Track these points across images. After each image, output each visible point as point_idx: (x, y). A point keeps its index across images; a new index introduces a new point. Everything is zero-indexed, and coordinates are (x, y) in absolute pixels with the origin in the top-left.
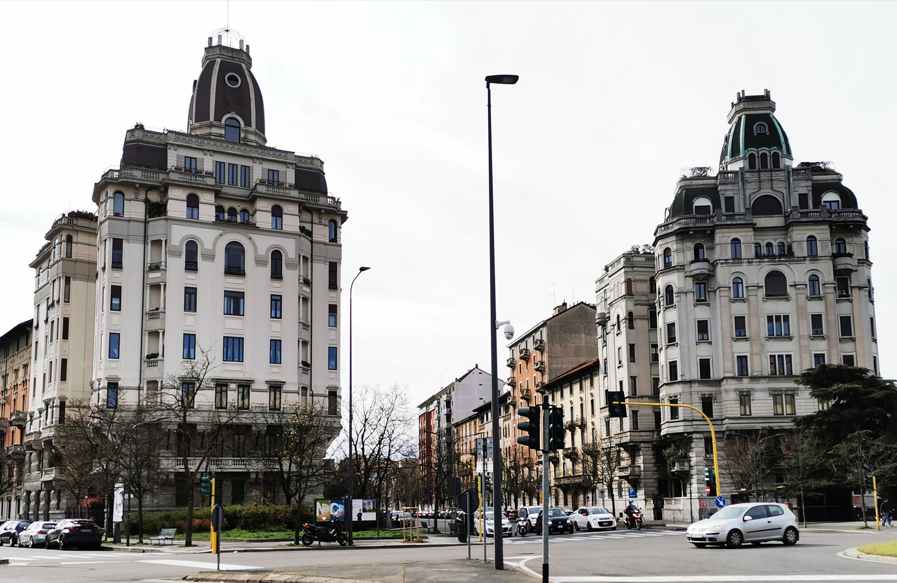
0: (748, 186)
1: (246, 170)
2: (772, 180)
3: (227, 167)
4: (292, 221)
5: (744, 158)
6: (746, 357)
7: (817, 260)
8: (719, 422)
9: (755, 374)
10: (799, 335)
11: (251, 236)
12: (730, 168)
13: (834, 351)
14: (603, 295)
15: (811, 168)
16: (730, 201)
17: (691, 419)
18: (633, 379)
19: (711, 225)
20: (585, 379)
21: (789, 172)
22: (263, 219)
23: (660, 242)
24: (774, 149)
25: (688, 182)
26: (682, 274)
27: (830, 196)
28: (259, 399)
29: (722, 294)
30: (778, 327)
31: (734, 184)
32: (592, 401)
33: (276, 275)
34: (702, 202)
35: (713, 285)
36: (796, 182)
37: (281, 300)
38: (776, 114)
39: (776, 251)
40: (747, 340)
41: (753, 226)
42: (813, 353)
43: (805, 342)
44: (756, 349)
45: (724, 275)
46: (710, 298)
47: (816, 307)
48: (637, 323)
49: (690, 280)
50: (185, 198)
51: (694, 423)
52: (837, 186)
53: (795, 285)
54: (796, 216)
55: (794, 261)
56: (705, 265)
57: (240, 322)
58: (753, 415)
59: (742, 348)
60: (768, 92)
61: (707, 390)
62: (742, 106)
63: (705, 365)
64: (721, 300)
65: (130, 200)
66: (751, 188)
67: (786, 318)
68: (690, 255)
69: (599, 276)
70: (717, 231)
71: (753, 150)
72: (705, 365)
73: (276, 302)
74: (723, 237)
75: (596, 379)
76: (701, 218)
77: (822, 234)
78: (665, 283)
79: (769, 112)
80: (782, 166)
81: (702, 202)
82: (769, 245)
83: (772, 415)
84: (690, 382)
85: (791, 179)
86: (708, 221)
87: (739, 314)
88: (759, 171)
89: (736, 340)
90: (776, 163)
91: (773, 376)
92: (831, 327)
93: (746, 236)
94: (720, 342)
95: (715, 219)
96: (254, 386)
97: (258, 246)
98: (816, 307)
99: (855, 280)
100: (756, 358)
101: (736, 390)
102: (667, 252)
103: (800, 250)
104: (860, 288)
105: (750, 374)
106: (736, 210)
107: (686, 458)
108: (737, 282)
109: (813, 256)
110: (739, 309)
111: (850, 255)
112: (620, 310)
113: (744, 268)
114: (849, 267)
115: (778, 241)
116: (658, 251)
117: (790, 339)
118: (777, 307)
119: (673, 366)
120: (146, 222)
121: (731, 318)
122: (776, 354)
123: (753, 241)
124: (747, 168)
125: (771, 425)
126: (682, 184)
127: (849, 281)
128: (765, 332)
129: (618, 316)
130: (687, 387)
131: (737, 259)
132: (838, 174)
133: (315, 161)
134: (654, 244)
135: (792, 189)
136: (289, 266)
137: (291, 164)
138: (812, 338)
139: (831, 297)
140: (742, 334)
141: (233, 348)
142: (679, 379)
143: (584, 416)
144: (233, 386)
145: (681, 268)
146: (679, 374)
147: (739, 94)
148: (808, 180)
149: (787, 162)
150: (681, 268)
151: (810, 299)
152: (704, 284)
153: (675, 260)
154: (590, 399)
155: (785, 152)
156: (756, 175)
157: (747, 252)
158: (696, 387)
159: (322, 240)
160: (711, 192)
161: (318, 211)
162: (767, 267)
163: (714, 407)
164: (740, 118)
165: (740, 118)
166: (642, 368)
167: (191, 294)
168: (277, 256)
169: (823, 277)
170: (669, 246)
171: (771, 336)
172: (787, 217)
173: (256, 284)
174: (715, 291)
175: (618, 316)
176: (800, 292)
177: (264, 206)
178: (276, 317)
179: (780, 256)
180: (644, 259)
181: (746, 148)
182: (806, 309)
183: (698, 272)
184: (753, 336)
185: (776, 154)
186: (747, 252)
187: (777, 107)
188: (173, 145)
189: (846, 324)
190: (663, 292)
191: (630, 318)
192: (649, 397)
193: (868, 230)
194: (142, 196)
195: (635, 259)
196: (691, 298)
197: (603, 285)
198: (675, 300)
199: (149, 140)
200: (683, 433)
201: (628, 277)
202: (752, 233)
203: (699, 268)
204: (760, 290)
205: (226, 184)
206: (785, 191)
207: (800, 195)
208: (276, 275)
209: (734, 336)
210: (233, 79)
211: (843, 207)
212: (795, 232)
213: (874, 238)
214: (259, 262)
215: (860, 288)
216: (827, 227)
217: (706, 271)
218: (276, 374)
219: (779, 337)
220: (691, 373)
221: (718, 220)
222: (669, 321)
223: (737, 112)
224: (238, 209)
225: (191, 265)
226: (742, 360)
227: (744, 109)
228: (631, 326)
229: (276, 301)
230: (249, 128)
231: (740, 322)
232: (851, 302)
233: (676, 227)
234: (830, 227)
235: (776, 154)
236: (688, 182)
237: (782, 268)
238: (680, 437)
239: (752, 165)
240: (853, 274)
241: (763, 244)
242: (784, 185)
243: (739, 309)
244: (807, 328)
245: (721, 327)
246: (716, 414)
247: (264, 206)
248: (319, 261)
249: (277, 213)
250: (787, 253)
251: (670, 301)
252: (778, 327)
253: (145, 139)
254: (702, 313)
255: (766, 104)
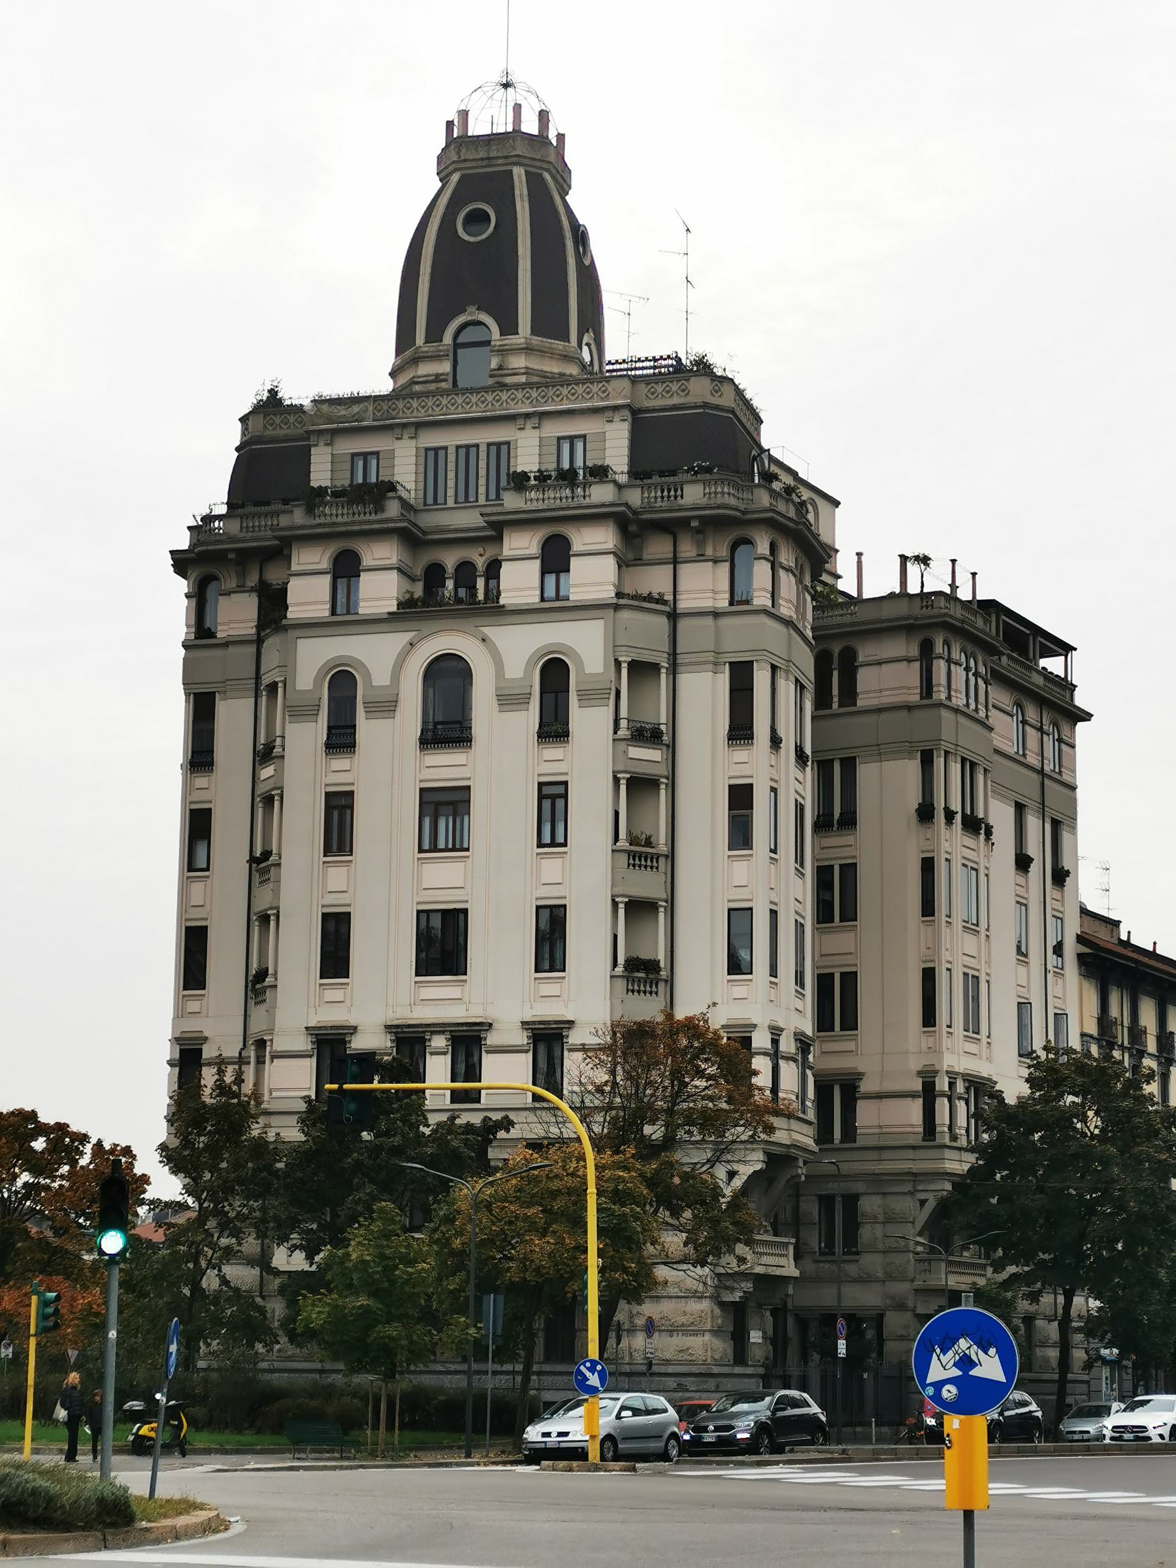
1: (501, 450)
3: (452, 458)
4: (593, 573)
11: (487, 631)
22: (520, 581)
28: (506, 1075)
33: (553, 729)
37: (565, 796)
50: (325, 564)
57: (460, 866)
65: (228, 594)
73: (553, 798)
96: (492, 1039)
97: (503, 655)
120: (259, 641)
133: (727, 389)
136: (584, 696)
137: (616, 408)
141: (442, 944)
144: (439, 1041)
159: (706, 603)
161: (684, 523)
167: (339, 808)
168: (555, 673)
173: (502, 758)
177: (523, 544)
178: (553, 844)
188: (320, 433)
194: (253, 580)
199: (279, 432)
205: (451, 503)
207: (517, 333)
208: (553, 729)
210: (477, 219)
214: (509, 700)
218: (551, 1001)
224: (481, 563)
225: (341, 739)
229: (553, 798)
230: (513, 340)
247: (523, 544)
248: (697, 665)
249: (555, 558)
253: (270, 432)
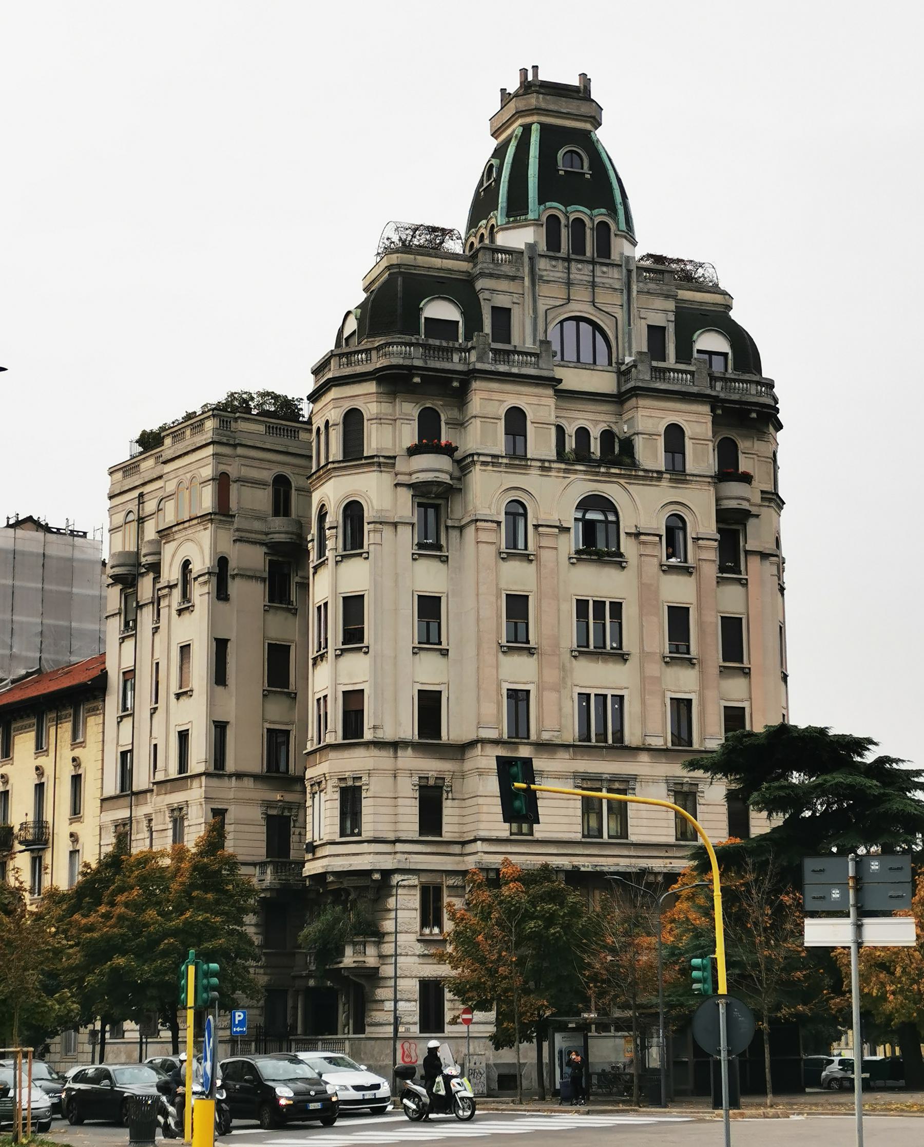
0: (543, 290)
2: (593, 285)
5: (537, 223)
6: (689, 701)
7: (685, 481)
8: (457, 849)
9: (546, 736)
10: (642, 650)
12: (504, 239)
13: (711, 694)
14: (133, 506)
15: (660, 267)
16: (502, 316)
17: (391, 836)
18: (220, 728)
19: (460, 367)
20: (58, 721)
21: (629, 271)
23: (334, 393)
24: (600, 216)
25: (408, 258)
26: (386, 479)
27: (710, 341)
29: (483, 536)
30: (599, 628)
31: (513, 278)
32: (76, 780)
34: (441, 310)
35: (456, 512)
36: (644, 297)
38: (600, 134)
39: (595, 447)
40: (530, 652)
41: (552, 382)
42: (670, 695)
43: (655, 668)
44: (551, 676)
45: (486, 492)
46: (450, 541)
47: (678, 590)
48: (235, 587)
49: (406, 496)
51: (399, 847)
52: (719, 318)
53: (637, 535)
54: (642, 376)
55: (637, 477)
56: (443, 462)
58: (633, 838)
59: (519, 671)
60: (585, 79)
61: (432, 766)
62: (533, 100)
63: (429, 705)
64: (477, 551)
66: (550, 295)
67: (617, 607)
68: (409, 435)
69: (123, 456)
70: (476, 385)
71: (555, 208)
72: (429, 705)
74: (488, 402)
75: (93, 724)
76: (440, 349)
77: (697, 424)
78: (341, 493)
79: (588, 126)
80: (615, 256)
81: (441, 310)
82: (583, 434)
83: (578, 837)
84: (395, 746)
85: (634, 288)
86: (456, 358)
87: (517, 590)
88: (568, 260)
89: (508, 651)
90: (604, 249)
91: (583, 745)
92: (705, 640)
93: (539, 407)
94: (471, 651)
95: (473, 356)
98: (678, 590)
99: (754, 538)
100: (550, 697)
101: (667, 780)
102: (353, 421)
103: (650, 454)
104: (764, 556)
105: (533, 737)
106: (516, 340)
107: (373, 933)
108: (517, 512)
109: (677, 472)
110: (518, 577)
111: (747, 478)
112: (198, 549)
113: (531, 480)
114: (745, 505)
115: (603, 427)
116: (330, 411)
117: (623, 658)
118: (599, 582)
119: (353, 704)
121: (498, 596)
122: (609, 693)
123: (552, 419)
124: (542, 247)
125: (577, 861)
126: (395, 259)
127: (740, 541)
128: (569, 637)
129: (186, 564)
130: (383, 759)
131: (517, 457)
132: (725, 293)
134: (314, 397)
135: (634, 311)
138: (670, 662)
139: (710, 571)
140: (683, 648)
142: (368, 735)
143: (48, 816)
145: (386, 463)
146: (368, 722)
147: (524, 72)
148: (667, 297)
149: (627, 249)
150: (386, 463)
151: (506, 557)
152: (436, 504)
153: (375, 440)
154: (67, 771)
155: (623, 226)
156: (561, 265)
157: (541, 444)
158: (408, 760)
160: (461, 289)
162: (581, 485)
163: (446, 811)
164: (527, 129)
165: (527, 129)
166: (245, 702)
169: (696, 522)
170: (358, 404)
171: (582, 651)
172: (623, 374)
174: (461, 529)
175: (186, 564)
176: (649, 550)
179: (600, 463)
180: (261, 428)
181: (541, 201)
182: (657, 592)
183: (429, 476)
184: (546, 646)
185: (604, 226)
186: (541, 444)
187: (605, 117)
189: (732, 630)
190: (334, 516)
191: (221, 574)
192: (256, 777)
193: (779, 426)
195: (242, 426)
196: (406, 538)
197: (136, 480)
198: (368, 539)
200: (368, 873)
201: (222, 468)
202: (551, 402)
203: (432, 467)
204: (563, 538)
206: (620, 314)
209: (504, 641)
211: (735, 368)
212: (641, 412)
213: (788, 443)
215: (764, 556)
216: (706, 409)
217: (445, 478)
219: (600, 653)
220: (397, 723)
221: (480, 359)
222: (350, 587)
223: (519, 114)
226: (518, 699)
227: (537, 111)
228: (222, 594)
231: (517, 606)
232: (745, 585)
233: (378, 362)
234: (713, 410)
235: (604, 226)
236: (408, 258)
237: (612, 491)
238: (361, 882)
239: (553, 242)
240: (751, 523)
241: (571, 430)
242: (618, 299)
243: (518, 577)
244: (660, 641)
245: (473, 617)
246: (449, 830)
250: (618, 454)
251: (354, 541)
252: (599, 628)
254: (429, 577)
255: (584, 109)
